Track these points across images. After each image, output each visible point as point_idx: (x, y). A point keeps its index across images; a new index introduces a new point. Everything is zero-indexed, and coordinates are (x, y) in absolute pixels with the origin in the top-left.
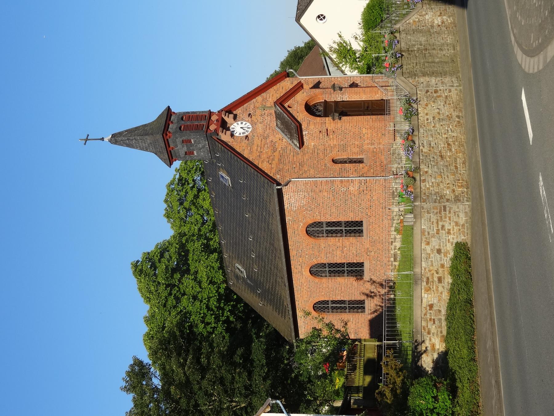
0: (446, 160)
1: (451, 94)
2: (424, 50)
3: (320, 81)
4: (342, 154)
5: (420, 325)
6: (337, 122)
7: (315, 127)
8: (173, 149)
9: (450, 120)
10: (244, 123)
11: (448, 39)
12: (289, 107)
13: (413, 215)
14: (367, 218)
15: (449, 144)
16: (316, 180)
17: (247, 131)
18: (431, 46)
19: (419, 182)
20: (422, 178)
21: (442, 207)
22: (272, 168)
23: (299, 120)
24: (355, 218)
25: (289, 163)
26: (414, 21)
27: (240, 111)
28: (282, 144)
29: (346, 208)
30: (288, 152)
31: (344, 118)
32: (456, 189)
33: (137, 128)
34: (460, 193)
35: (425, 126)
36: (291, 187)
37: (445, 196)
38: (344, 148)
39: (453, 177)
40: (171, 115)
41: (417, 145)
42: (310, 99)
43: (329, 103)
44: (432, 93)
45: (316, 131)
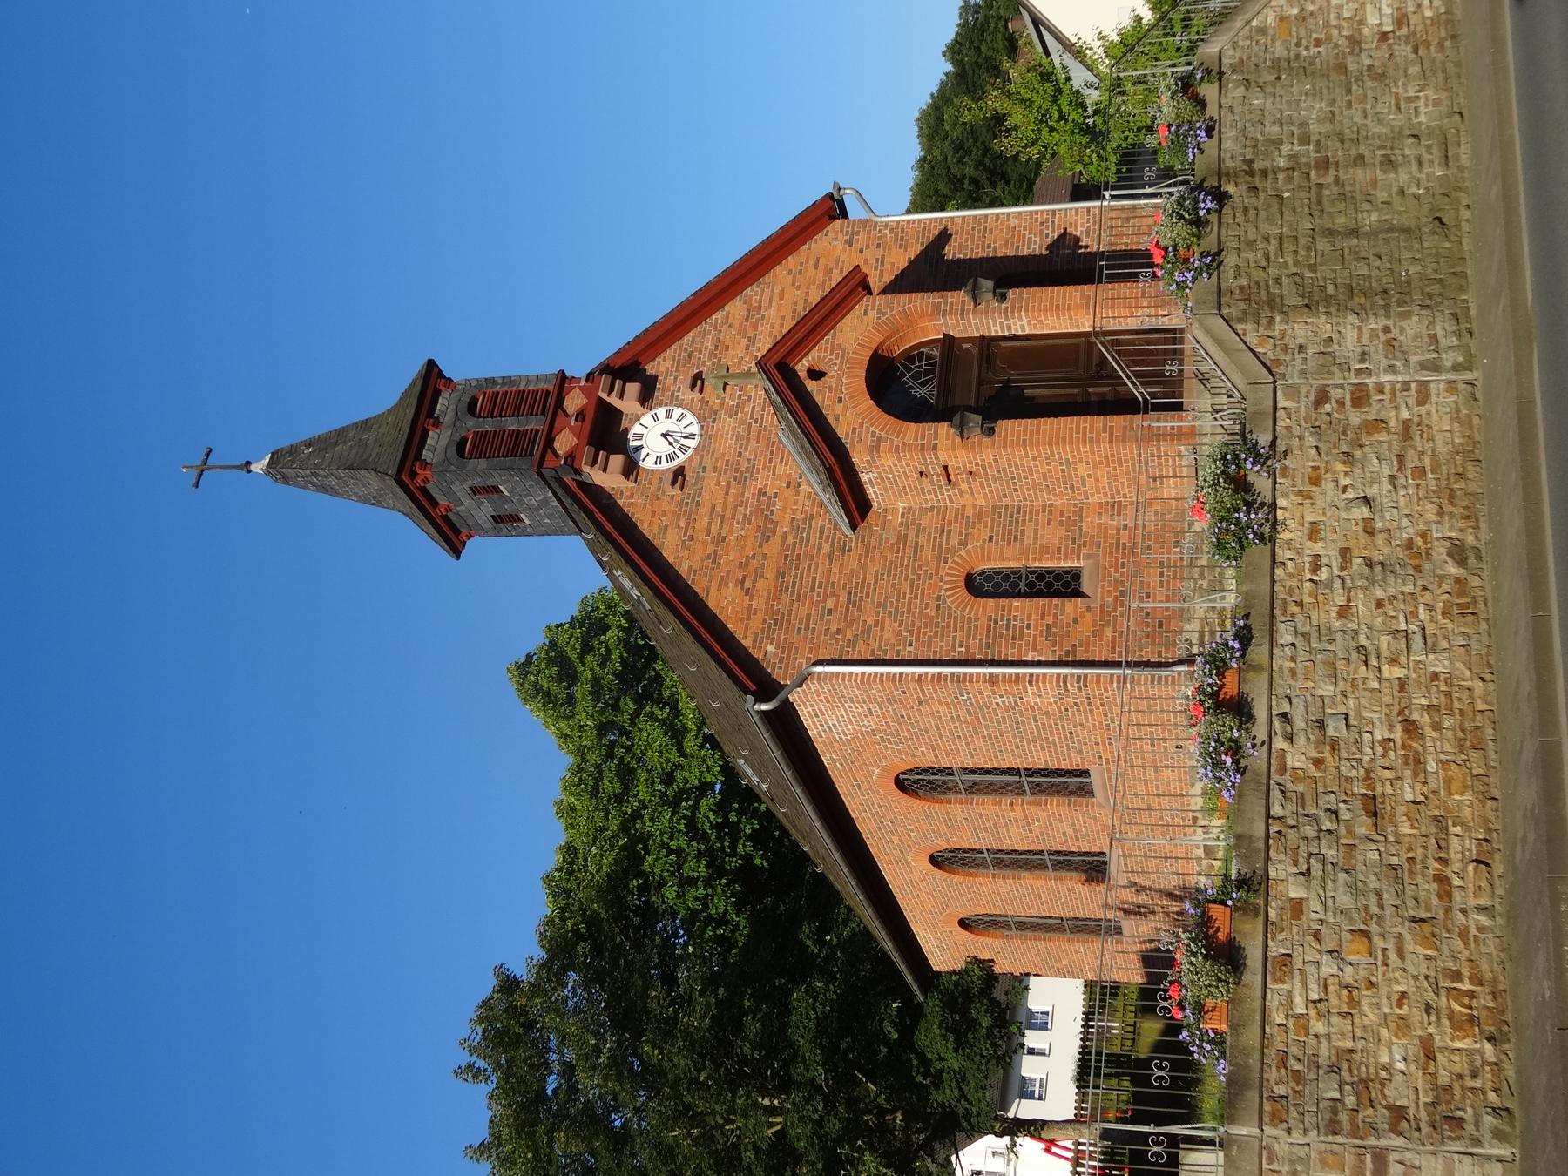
0: (1396, 834)
1: (1429, 414)
2: (1317, 166)
3: (946, 229)
4: (1002, 552)
6: (980, 444)
7: (900, 462)
8: (448, 509)
9: (1418, 569)
10: (677, 412)
11: (1422, 103)
12: (816, 375)
13: (1221, 1154)
15: (1410, 727)
16: (901, 674)
17: (683, 449)
18: (1346, 146)
19: (1259, 977)
21: (1368, 1158)
22: (751, 612)
23: (842, 431)
25: (813, 590)
27: (668, 363)
28: (796, 503)
30: (814, 541)
31: (1006, 426)
32: (1443, 1036)
34: (1457, 1069)
35: (1300, 604)
36: (817, 691)
37: (1383, 1085)
38: (1011, 521)
39: (1429, 952)
40: (437, 393)
41: (1260, 731)
42: (888, 338)
43: (960, 348)
44: (1341, 403)
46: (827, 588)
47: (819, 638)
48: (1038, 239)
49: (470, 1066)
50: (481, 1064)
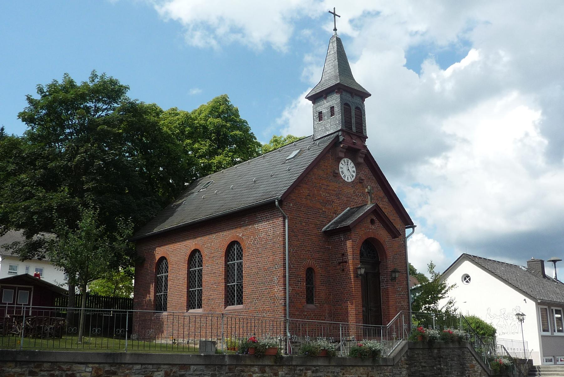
5: (43, 360)
14: (245, 309)
20: (267, 369)
24: (246, 295)
25: (308, 218)
26: (474, 365)
28: (330, 213)
29: (256, 284)
33: (343, 51)
45: (344, 249)
46: (308, 223)
47: (294, 220)
48: (400, 290)
49: (96, 76)
50: (96, 80)
